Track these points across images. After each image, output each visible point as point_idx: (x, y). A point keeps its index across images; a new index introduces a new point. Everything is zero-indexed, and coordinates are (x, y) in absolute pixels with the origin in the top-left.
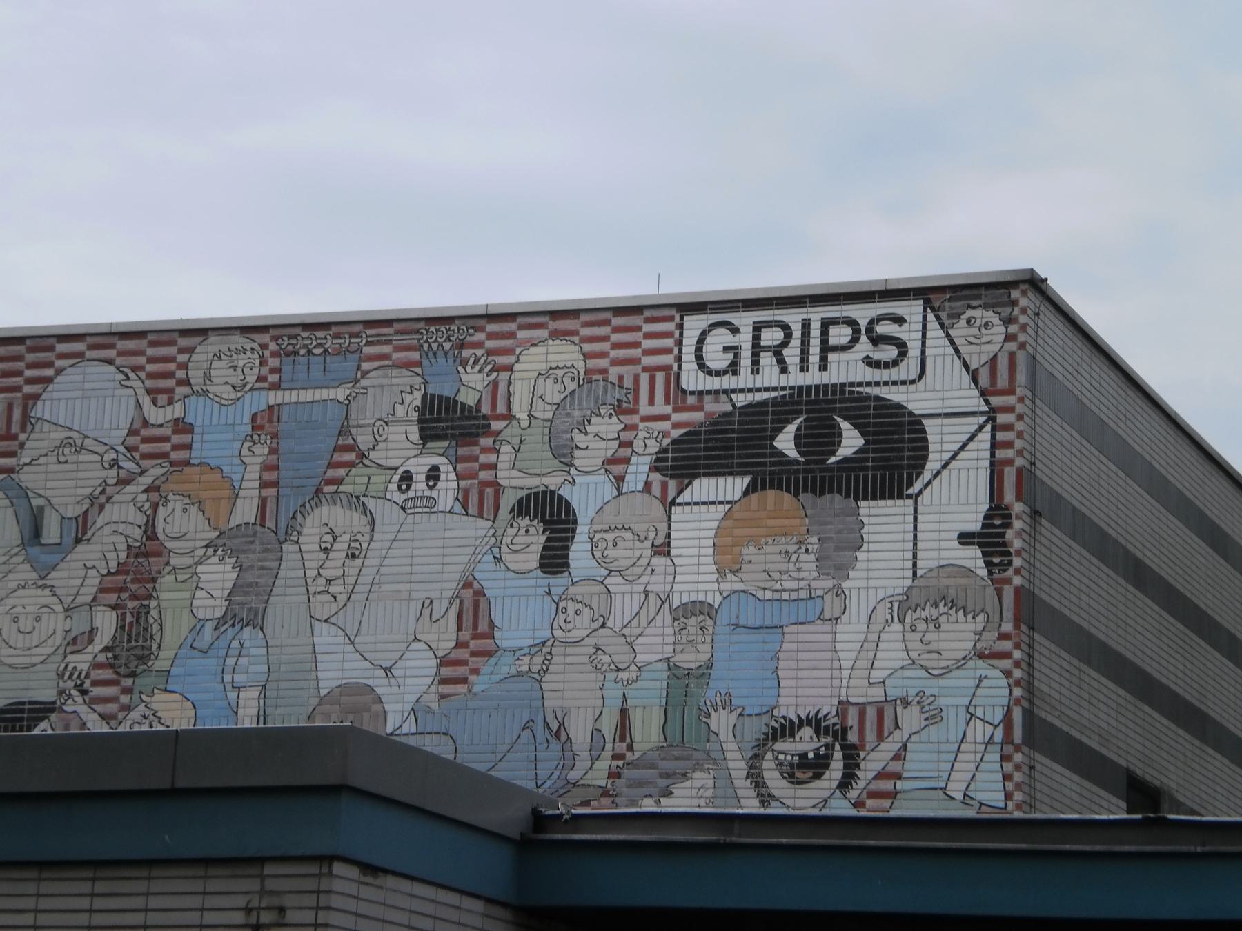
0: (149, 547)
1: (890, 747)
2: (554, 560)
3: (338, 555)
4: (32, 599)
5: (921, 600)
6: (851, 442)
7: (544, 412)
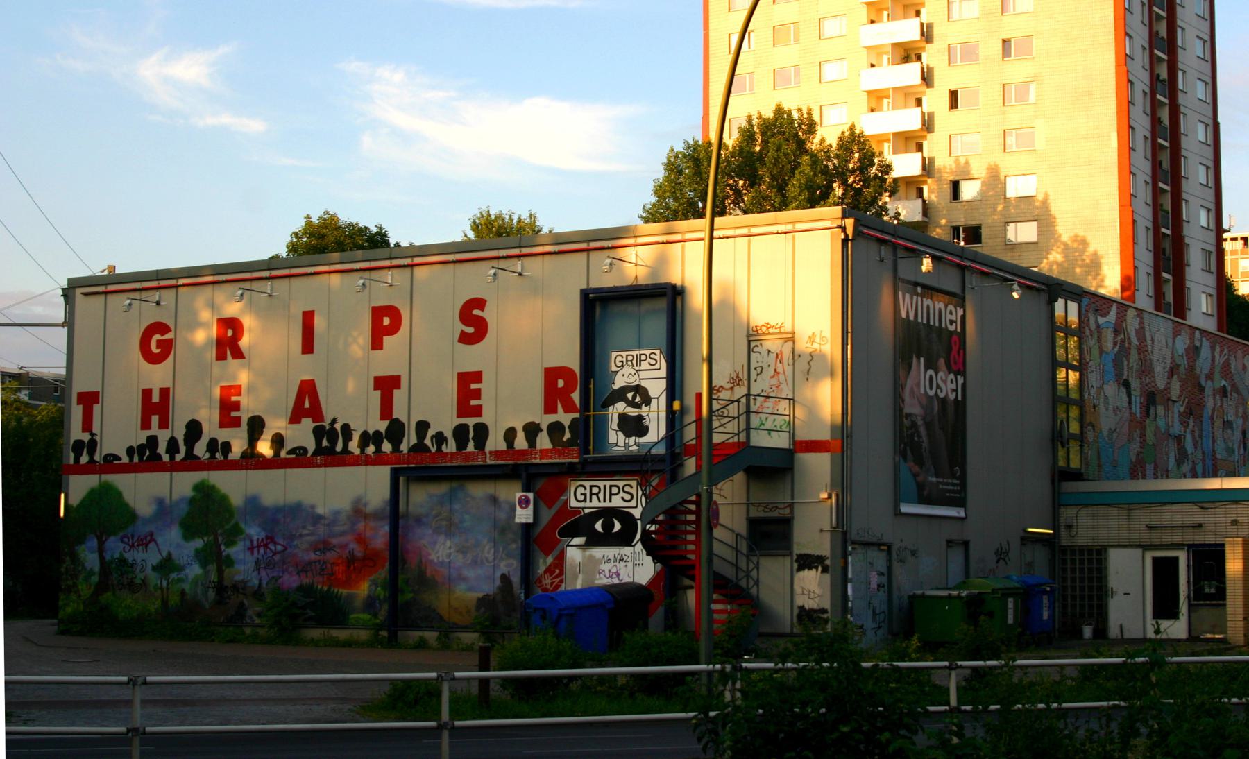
6: (617, 526)
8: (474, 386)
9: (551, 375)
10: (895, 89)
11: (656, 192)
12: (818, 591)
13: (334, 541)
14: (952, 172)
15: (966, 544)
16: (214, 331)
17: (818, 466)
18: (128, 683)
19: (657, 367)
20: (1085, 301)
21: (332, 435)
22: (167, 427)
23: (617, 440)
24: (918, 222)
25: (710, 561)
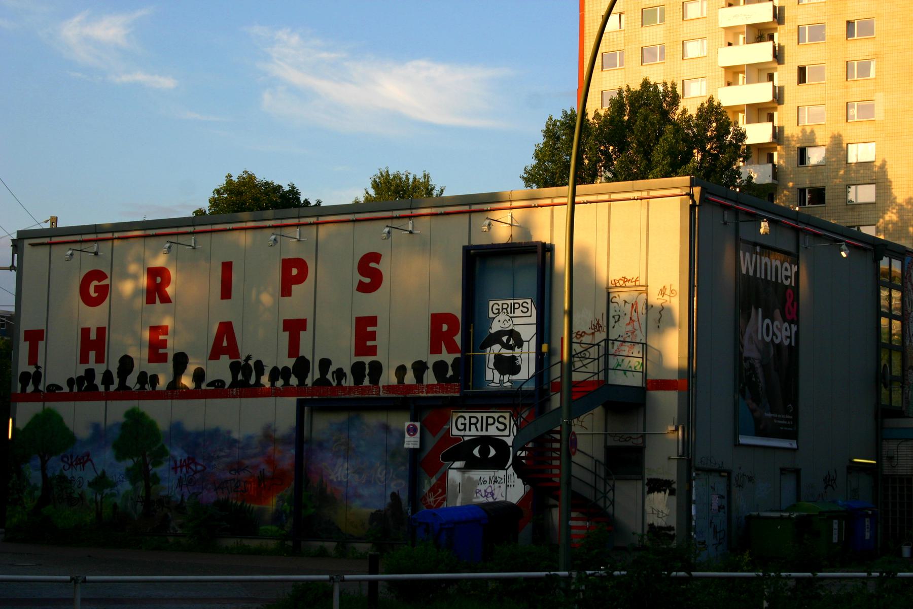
6: (493, 452)
8: (369, 329)
9: (437, 319)
10: (749, 65)
11: (537, 156)
12: (666, 511)
13: (247, 462)
14: (799, 140)
15: (797, 472)
16: (144, 281)
17: (667, 403)
18: (70, 581)
19: (528, 314)
20: (908, 259)
21: (246, 369)
22: (103, 362)
23: (493, 377)
24: (767, 185)
25: (569, 483)
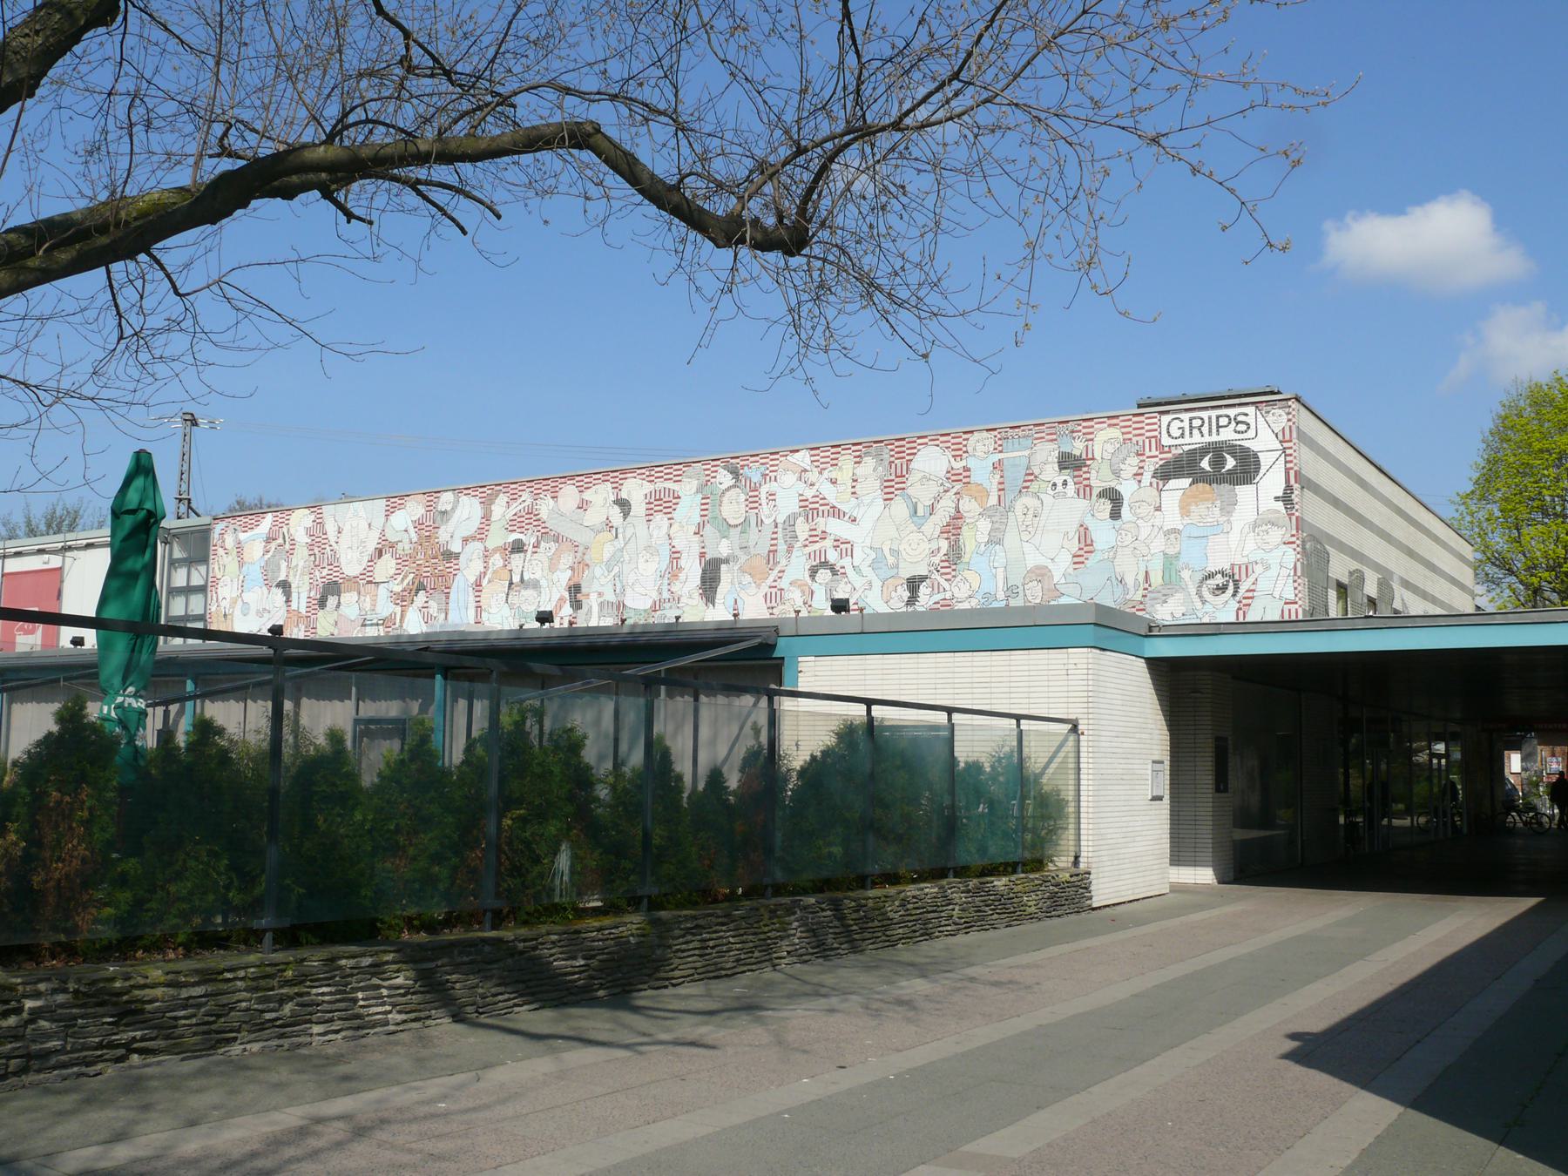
0: (958, 516)
1: (1251, 580)
2: (1115, 514)
3: (1030, 516)
4: (915, 537)
5: (1261, 523)
6: (1231, 463)
7: (1107, 456)
